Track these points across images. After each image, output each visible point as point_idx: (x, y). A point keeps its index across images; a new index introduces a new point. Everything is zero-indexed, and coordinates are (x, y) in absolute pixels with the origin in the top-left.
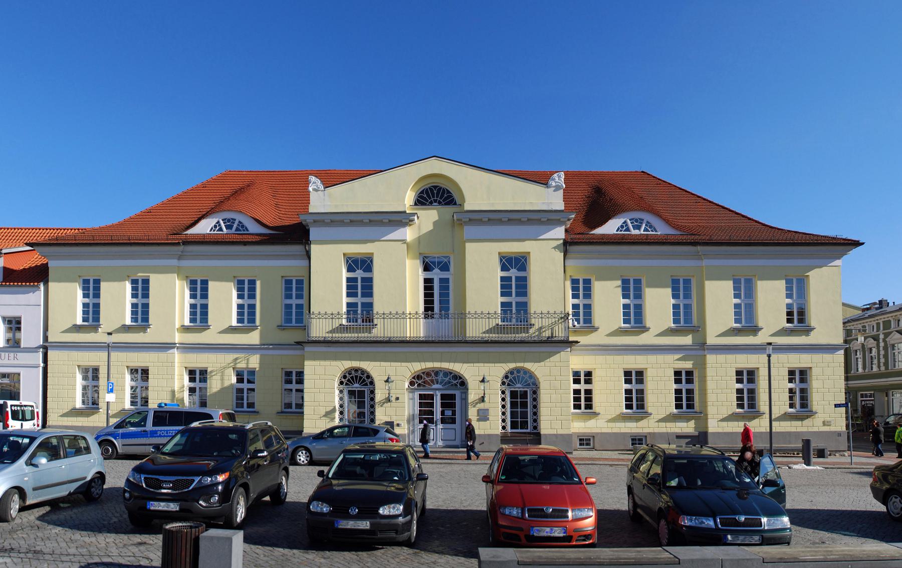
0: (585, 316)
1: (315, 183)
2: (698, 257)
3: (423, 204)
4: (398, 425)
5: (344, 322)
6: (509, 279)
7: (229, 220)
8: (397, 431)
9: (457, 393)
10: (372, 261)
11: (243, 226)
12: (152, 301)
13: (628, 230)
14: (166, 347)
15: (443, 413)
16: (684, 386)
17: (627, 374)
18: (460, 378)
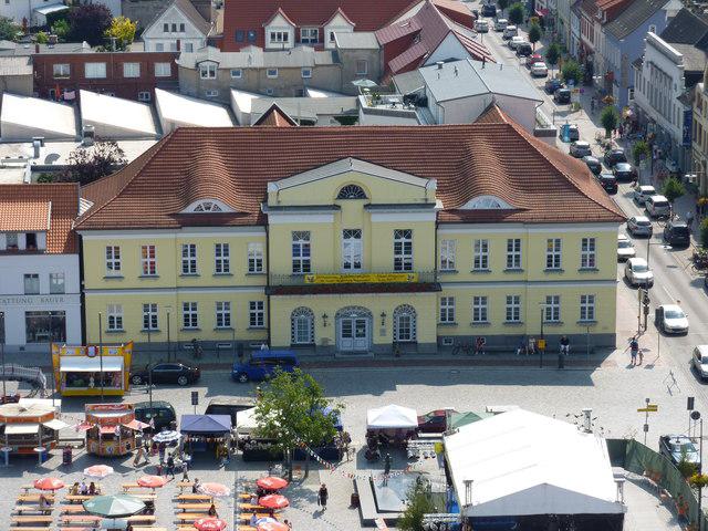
8: (330, 343)
9: (367, 319)
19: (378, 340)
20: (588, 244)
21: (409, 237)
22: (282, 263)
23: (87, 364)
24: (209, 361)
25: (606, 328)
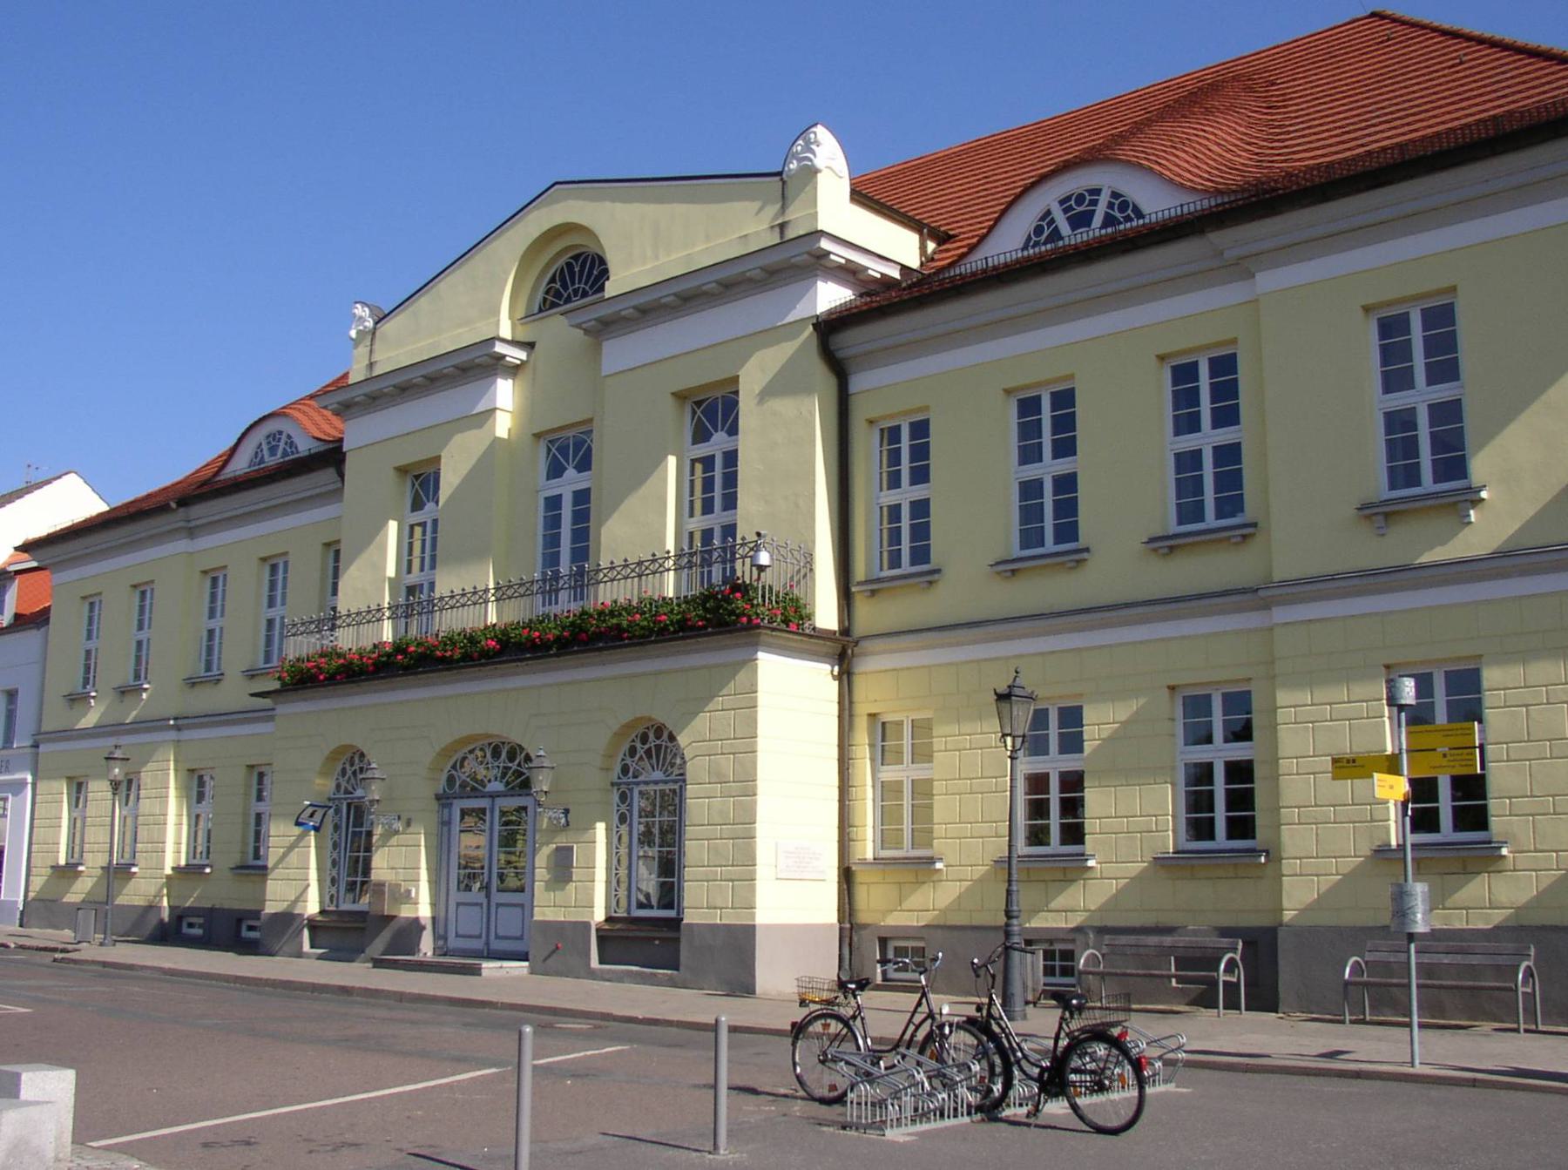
7: (1080, 199)
11: (1124, 206)
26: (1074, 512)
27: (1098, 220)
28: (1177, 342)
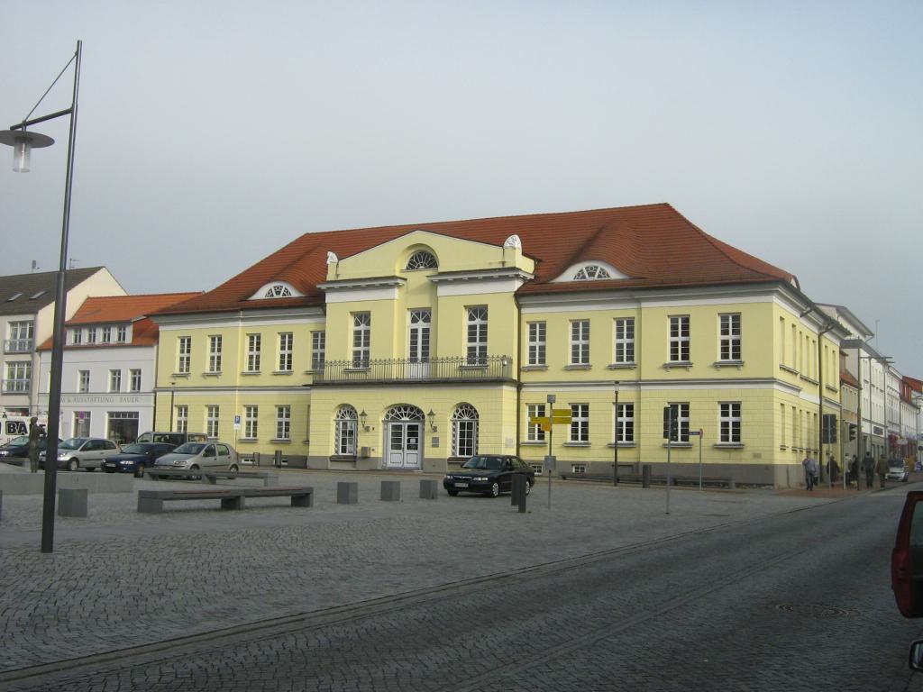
0: (539, 356)
1: (332, 257)
2: (638, 301)
3: (413, 268)
4: (373, 450)
5: (465, 364)
6: (475, 327)
7: (592, 269)
8: (373, 455)
9: (420, 425)
10: (430, 313)
11: (604, 273)
12: (549, 344)
13: (584, 277)
14: (233, 389)
15: (409, 441)
16: (731, 419)
17: (725, 407)
18: (416, 408)
19: (430, 452)
20: (732, 323)
21: (485, 318)
22: (341, 349)
23: (67, 424)
24: (142, 404)
25: (757, 456)
26: (588, 355)
27: (596, 276)
28: (576, 317)
